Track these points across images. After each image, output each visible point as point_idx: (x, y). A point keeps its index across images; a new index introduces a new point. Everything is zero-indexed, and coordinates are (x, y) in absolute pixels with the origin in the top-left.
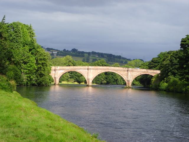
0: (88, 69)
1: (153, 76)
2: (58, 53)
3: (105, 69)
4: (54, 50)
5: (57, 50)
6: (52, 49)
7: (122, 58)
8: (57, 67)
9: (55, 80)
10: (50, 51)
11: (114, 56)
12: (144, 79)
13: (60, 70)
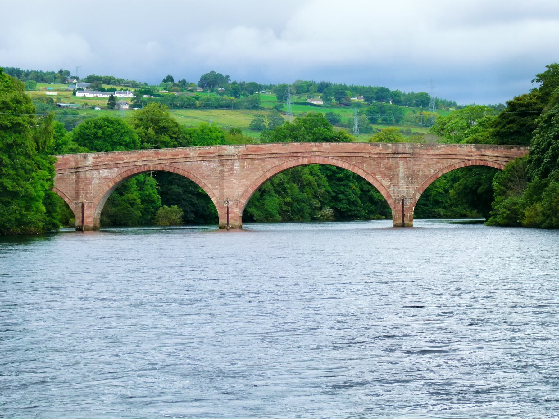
0: (221, 158)
1: (414, 220)
2: (139, 94)
3: (288, 156)
4: (119, 82)
5: (134, 85)
6: (108, 81)
7: (433, 104)
8: (85, 158)
9: (78, 214)
10: (103, 90)
11: (396, 98)
12: (479, 191)
13: (96, 167)
